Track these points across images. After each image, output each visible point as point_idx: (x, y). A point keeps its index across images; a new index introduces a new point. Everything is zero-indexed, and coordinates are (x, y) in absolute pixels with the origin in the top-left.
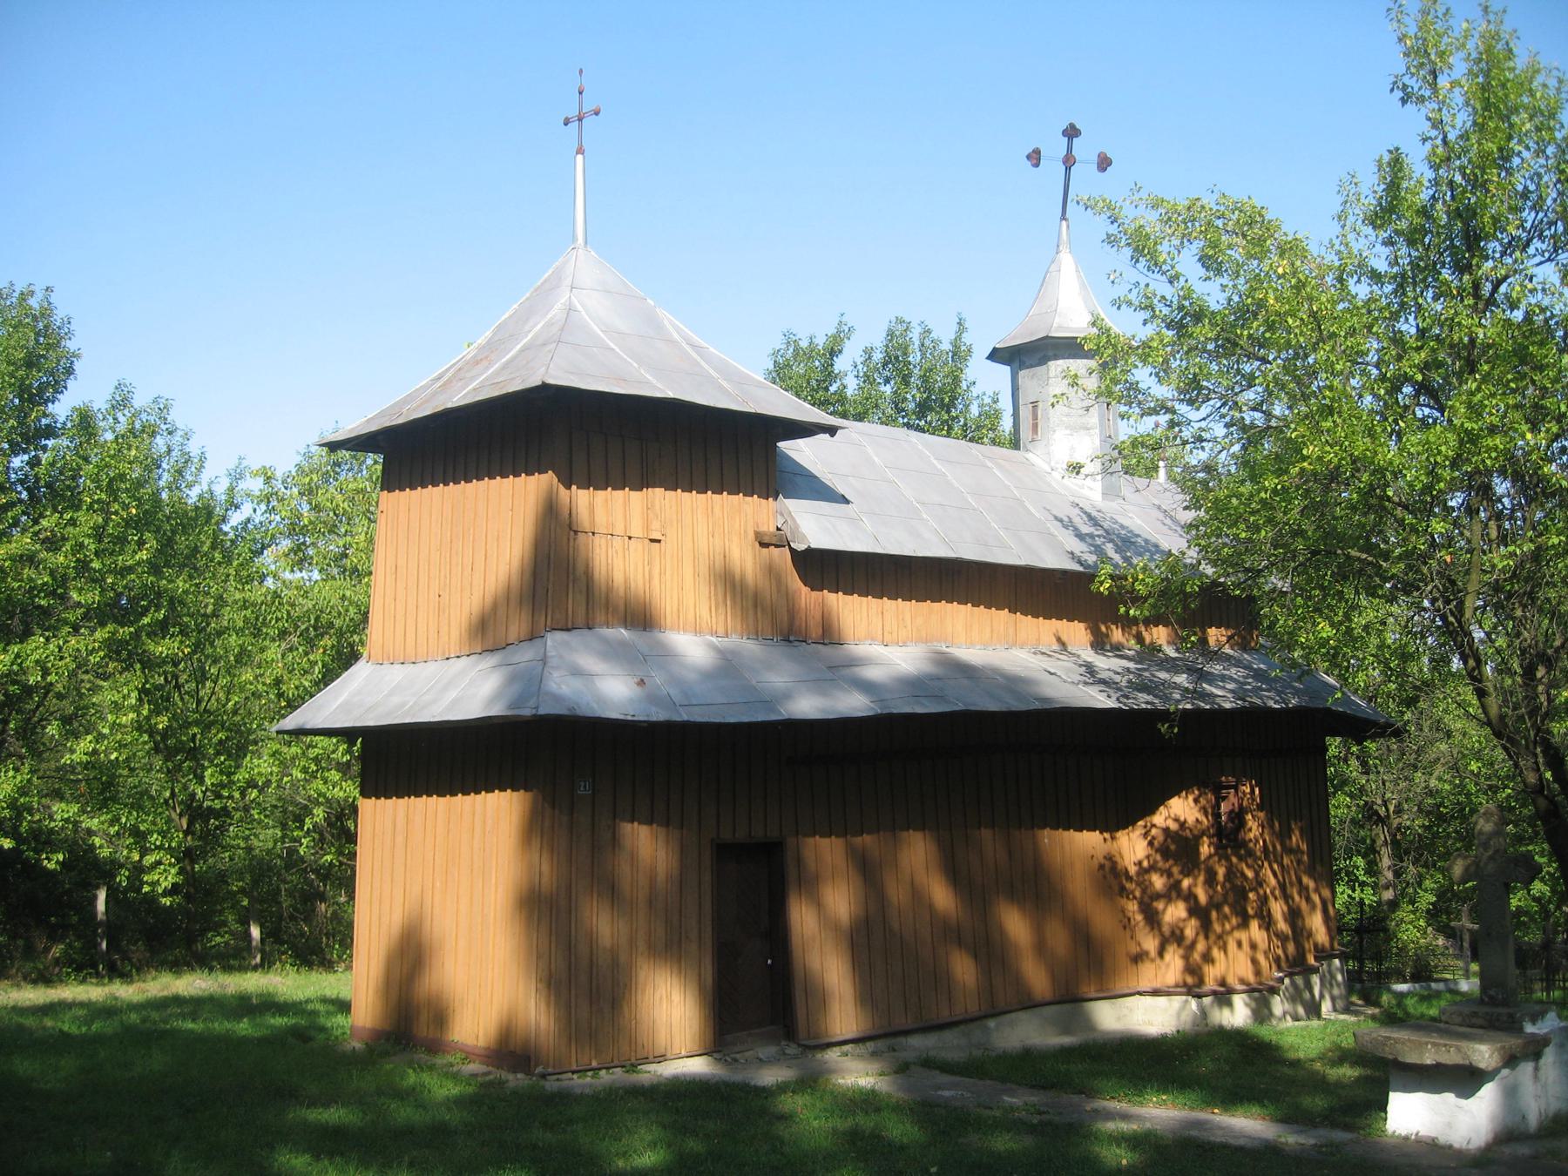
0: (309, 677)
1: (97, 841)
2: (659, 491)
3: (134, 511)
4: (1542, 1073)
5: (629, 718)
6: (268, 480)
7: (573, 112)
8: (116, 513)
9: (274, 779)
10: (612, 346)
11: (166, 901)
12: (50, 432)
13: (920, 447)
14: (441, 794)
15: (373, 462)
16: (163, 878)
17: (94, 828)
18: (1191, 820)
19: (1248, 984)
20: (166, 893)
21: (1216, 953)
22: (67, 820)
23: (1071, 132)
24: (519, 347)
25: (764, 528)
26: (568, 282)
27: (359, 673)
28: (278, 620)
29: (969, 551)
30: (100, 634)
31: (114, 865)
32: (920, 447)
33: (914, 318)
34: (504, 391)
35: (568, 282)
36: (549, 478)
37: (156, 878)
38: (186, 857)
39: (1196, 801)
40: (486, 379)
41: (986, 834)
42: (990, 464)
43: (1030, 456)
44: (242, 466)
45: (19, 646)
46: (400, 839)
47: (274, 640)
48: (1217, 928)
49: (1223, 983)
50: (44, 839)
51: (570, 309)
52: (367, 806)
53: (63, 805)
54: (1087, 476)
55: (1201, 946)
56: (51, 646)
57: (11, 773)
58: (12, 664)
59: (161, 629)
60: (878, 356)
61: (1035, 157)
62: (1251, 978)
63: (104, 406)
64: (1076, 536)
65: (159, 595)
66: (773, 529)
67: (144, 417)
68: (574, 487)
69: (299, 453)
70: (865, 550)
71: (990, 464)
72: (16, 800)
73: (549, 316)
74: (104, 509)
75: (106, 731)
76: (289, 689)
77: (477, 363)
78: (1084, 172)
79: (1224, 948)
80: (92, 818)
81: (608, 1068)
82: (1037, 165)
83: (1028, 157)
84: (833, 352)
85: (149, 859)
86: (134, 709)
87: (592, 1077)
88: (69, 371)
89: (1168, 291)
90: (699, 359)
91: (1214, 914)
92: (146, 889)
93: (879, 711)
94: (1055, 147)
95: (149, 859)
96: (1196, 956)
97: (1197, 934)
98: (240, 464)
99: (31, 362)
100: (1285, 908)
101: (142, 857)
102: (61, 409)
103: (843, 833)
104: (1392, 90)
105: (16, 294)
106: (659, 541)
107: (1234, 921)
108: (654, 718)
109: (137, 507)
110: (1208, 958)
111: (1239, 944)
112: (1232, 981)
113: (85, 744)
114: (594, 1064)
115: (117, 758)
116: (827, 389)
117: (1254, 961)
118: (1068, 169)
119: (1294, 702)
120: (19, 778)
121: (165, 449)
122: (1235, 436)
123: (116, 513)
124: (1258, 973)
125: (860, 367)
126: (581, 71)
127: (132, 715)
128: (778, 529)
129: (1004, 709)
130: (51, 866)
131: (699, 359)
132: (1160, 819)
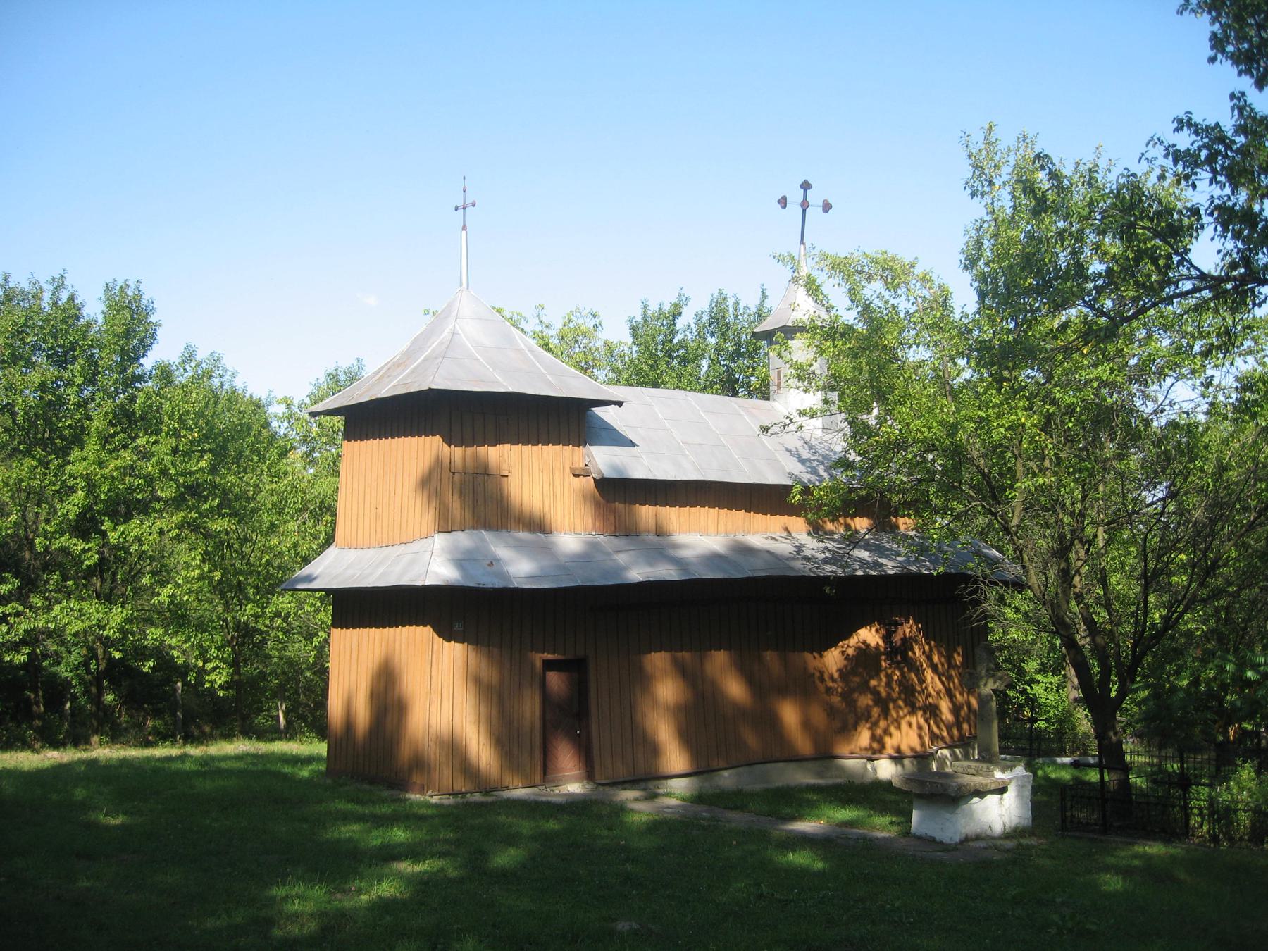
0: (316, 542)
1: (175, 653)
2: (507, 446)
3: (196, 435)
4: (1004, 803)
5: (481, 586)
6: (288, 406)
7: (460, 204)
9: (292, 611)
10: (479, 357)
11: (221, 693)
12: (141, 378)
13: (694, 404)
14: (377, 627)
15: (338, 422)
16: (219, 678)
17: (173, 645)
18: (873, 644)
19: (916, 752)
20: (221, 687)
21: (892, 729)
22: (156, 640)
23: (806, 186)
24: (422, 358)
25: (576, 466)
26: (454, 314)
27: (332, 552)
28: (295, 503)
29: (714, 474)
30: (177, 518)
31: (186, 669)
32: (694, 404)
33: (728, 292)
34: (408, 391)
35: (454, 314)
36: (437, 440)
37: (214, 678)
38: (235, 664)
39: (877, 631)
40: (401, 379)
42: (742, 413)
43: (775, 404)
44: (271, 397)
45: (123, 526)
46: (354, 656)
47: (292, 517)
48: (894, 714)
49: (898, 750)
50: (141, 653)
51: (454, 333)
52: (336, 632)
53: (153, 629)
54: (772, 434)
55: (882, 724)
56: (144, 527)
57: (120, 609)
58: (119, 537)
59: (217, 512)
60: (705, 318)
61: (783, 202)
62: (918, 748)
63: (178, 361)
64: (799, 461)
65: (215, 487)
66: (582, 465)
67: (204, 365)
68: (452, 446)
69: (311, 384)
70: (645, 478)
71: (742, 413)
72: (124, 627)
73: (442, 337)
74: (176, 434)
75: (180, 581)
76: (303, 550)
77: (399, 366)
78: (814, 212)
79: (899, 728)
80: (172, 638)
81: (471, 793)
82: (784, 207)
83: (779, 202)
84: (675, 314)
85: (209, 666)
86: (200, 567)
87: (462, 798)
88: (153, 336)
89: (825, 316)
90: (535, 362)
91: (891, 706)
92: (207, 685)
93: (641, 580)
94: (796, 196)
95: (209, 666)
96: (879, 732)
97: (879, 716)
98: (269, 395)
99: (128, 334)
100: (950, 705)
101: (204, 664)
102: (148, 362)
103: (669, 649)
104: (965, 188)
105: (118, 288)
106: (507, 476)
107: (906, 711)
108: (496, 586)
109: (198, 432)
110: (887, 732)
111: (910, 725)
112: (904, 748)
113: (167, 590)
114: (463, 790)
115: (188, 600)
116: (671, 341)
117: (920, 737)
118: (804, 211)
119: (941, 569)
120: (125, 613)
121: (219, 384)
123: (185, 436)
124: (923, 745)
125: (693, 326)
126: (464, 178)
127: (197, 571)
128: (586, 465)
129: (726, 577)
130: (146, 670)
131: (535, 362)
132: (853, 641)
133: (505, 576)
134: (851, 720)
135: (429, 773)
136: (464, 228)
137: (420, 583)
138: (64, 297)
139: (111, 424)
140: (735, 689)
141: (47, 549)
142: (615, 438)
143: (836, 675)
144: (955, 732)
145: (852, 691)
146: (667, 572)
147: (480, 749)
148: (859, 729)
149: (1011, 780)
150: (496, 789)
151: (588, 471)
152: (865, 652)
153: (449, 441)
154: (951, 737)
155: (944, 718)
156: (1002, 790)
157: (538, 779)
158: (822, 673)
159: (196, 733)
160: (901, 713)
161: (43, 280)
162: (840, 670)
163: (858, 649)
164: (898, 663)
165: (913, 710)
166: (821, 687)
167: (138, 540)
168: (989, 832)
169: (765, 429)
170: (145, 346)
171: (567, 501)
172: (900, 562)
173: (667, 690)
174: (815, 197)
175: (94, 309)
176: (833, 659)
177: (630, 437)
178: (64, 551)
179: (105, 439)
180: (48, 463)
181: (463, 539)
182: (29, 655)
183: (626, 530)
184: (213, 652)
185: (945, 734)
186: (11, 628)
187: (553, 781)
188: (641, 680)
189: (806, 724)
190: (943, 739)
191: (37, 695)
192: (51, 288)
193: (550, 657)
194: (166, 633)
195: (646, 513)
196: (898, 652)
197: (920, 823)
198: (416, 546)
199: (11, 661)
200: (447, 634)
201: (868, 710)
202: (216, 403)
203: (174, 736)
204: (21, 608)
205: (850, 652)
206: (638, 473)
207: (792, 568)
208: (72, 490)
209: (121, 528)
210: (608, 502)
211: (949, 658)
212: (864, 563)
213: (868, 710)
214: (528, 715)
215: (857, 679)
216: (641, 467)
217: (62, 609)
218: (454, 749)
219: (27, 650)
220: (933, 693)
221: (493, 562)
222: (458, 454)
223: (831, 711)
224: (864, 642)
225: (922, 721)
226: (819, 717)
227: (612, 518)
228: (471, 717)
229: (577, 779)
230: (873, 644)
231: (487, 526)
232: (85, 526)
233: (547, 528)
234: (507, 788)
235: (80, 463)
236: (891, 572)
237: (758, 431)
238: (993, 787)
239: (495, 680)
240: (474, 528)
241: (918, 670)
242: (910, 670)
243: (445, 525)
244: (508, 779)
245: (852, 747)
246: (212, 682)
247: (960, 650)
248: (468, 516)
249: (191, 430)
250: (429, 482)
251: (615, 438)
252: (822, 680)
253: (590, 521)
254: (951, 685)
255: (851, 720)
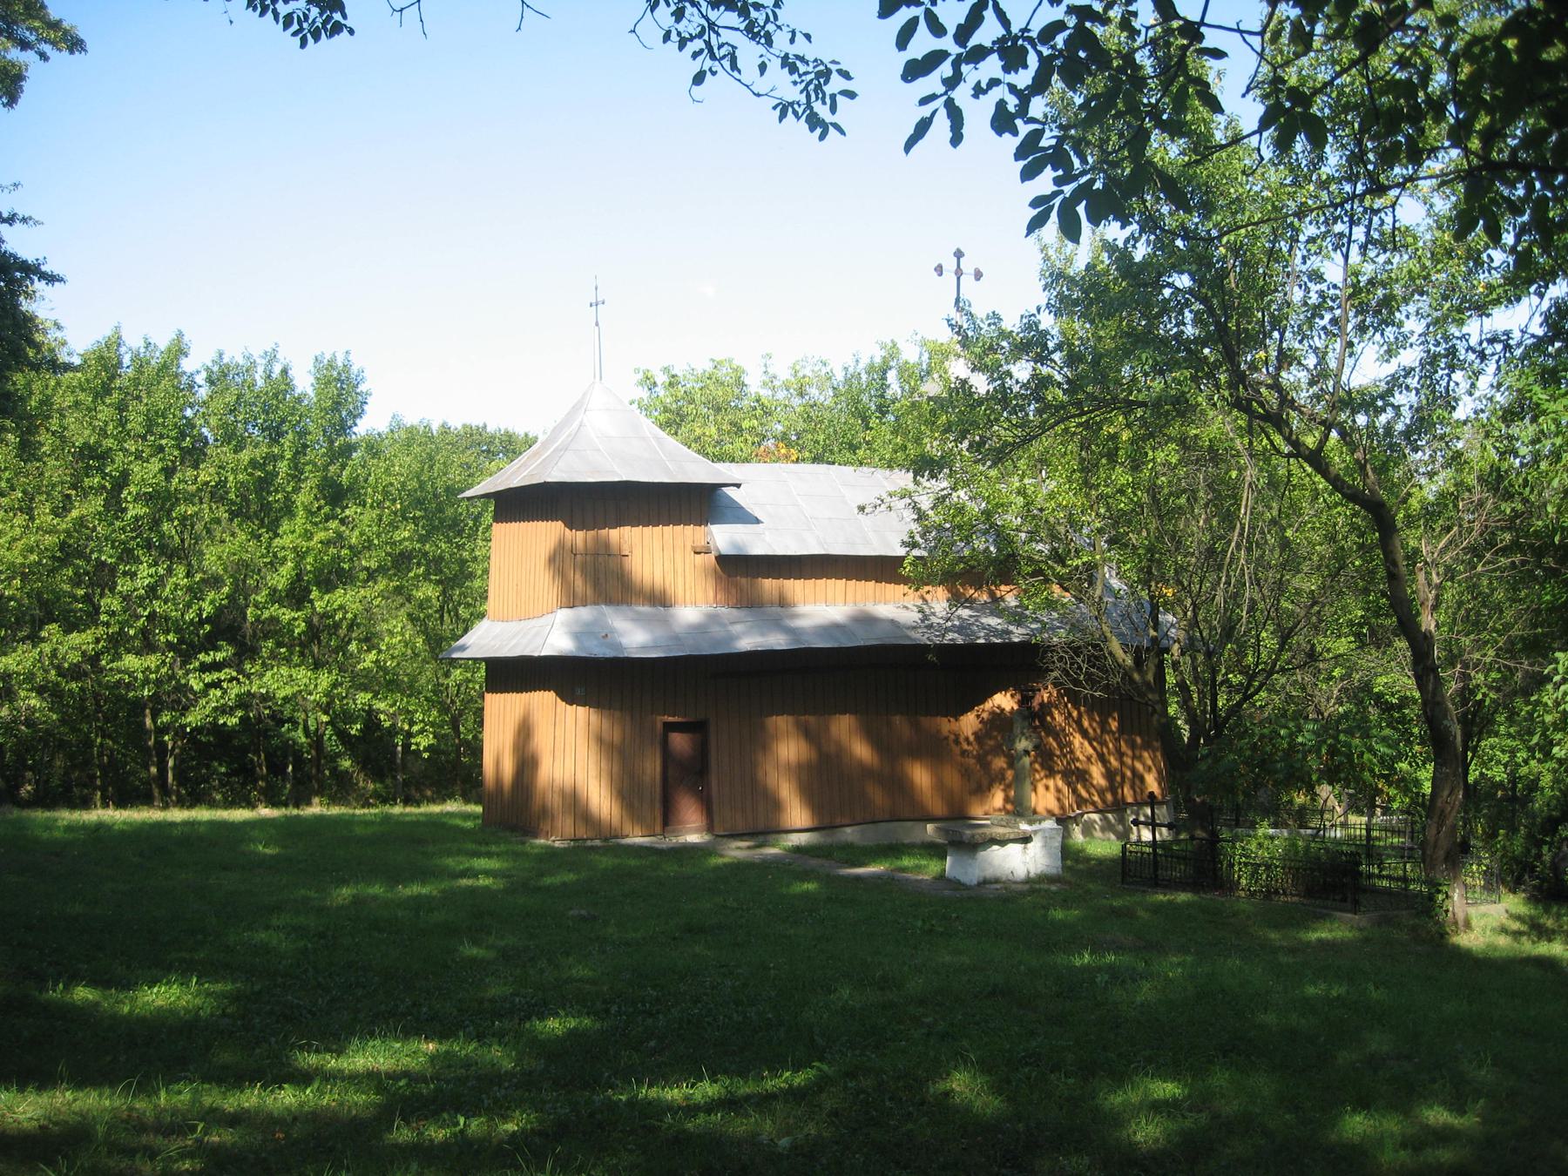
1: (382, 717)
2: (628, 528)
8: (388, 508)
18: (1008, 709)
20: (426, 749)
23: (959, 254)
39: (1012, 696)
41: (897, 720)
52: (488, 696)
62: (1057, 811)
75: (384, 648)
78: (967, 280)
79: (1035, 790)
82: (941, 274)
85: (415, 728)
92: (413, 747)
94: (950, 264)
95: (415, 728)
99: (337, 405)
107: (1042, 774)
111: (1047, 788)
113: (372, 656)
118: (958, 279)
122: (1433, 348)
124: (1062, 807)
130: (353, 732)
132: (988, 705)
133: (619, 646)
134: (985, 783)
135: (552, 820)
136: (597, 324)
137: (536, 654)
138: (277, 369)
139: (316, 499)
140: (861, 750)
141: (258, 619)
142: (742, 516)
143: (972, 738)
144: (1109, 797)
145: (987, 753)
146: (776, 641)
147: (601, 799)
148: (993, 791)
149: (1035, 832)
150: (616, 837)
151: (709, 548)
152: (998, 717)
153: (570, 525)
154: (1104, 801)
155: (1095, 782)
156: (1026, 840)
157: (658, 829)
158: (957, 736)
159: (418, 796)
160: (1037, 776)
161: (257, 354)
162: (975, 734)
163: (992, 713)
164: (1035, 728)
165: (1051, 773)
166: (956, 750)
167: (341, 607)
168: (1010, 877)
169: (862, 509)
170: (356, 415)
171: (687, 574)
172: (1032, 630)
173: (789, 749)
174: (968, 265)
175: (304, 383)
176: (969, 723)
177: (757, 514)
178: (274, 620)
179: (310, 513)
180: (260, 536)
181: (585, 613)
182: (241, 718)
183: (749, 603)
184: (419, 716)
185: (1096, 798)
186: (225, 692)
187: (673, 831)
188: (760, 742)
189: (939, 785)
190: (1094, 803)
191: (259, 757)
192: (264, 362)
193: (671, 719)
194: (375, 696)
195: (769, 585)
196: (1034, 717)
197: (952, 866)
198: (542, 621)
199: (225, 723)
200: (569, 697)
201: (1002, 773)
202: (431, 467)
203: (395, 800)
204: (234, 674)
205: (985, 715)
206: (758, 549)
207: (909, 637)
208: (284, 561)
209: (327, 597)
210: (729, 576)
211: (1104, 725)
212: (992, 631)
213: (1002, 773)
214: (648, 771)
215: (992, 743)
216: (760, 542)
217: (273, 675)
218: (574, 803)
219: (239, 713)
220: (1081, 757)
221: (606, 636)
222: (579, 537)
223: (966, 773)
224: (999, 707)
225: (1060, 783)
226: (952, 778)
227: (734, 591)
228: (593, 772)
229: (697, 831)
230: (1008, 709)
231: (609, 601)
232: (296, 595)
233: (668, 603)
234: (627, 836)
235: (289, 536)
236: (1016, 640)
237: (856, 511)
238: (1012, 837)
239: (617, 738)
240: (595, 603)
241: (1058, 735)
242: (1048, 735)
243: (571, 600)
244: (628, 828)
245: (987, 808)
246: (418, 744)
247: (1116, 715)
248: (589, 592)
249: (394, 501)
250: (559, 559)
251: (742, 516)
252: (957, 742)
253: (711, 594)
254: (1105, 750)
255: (985, 783)
